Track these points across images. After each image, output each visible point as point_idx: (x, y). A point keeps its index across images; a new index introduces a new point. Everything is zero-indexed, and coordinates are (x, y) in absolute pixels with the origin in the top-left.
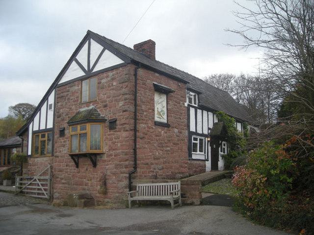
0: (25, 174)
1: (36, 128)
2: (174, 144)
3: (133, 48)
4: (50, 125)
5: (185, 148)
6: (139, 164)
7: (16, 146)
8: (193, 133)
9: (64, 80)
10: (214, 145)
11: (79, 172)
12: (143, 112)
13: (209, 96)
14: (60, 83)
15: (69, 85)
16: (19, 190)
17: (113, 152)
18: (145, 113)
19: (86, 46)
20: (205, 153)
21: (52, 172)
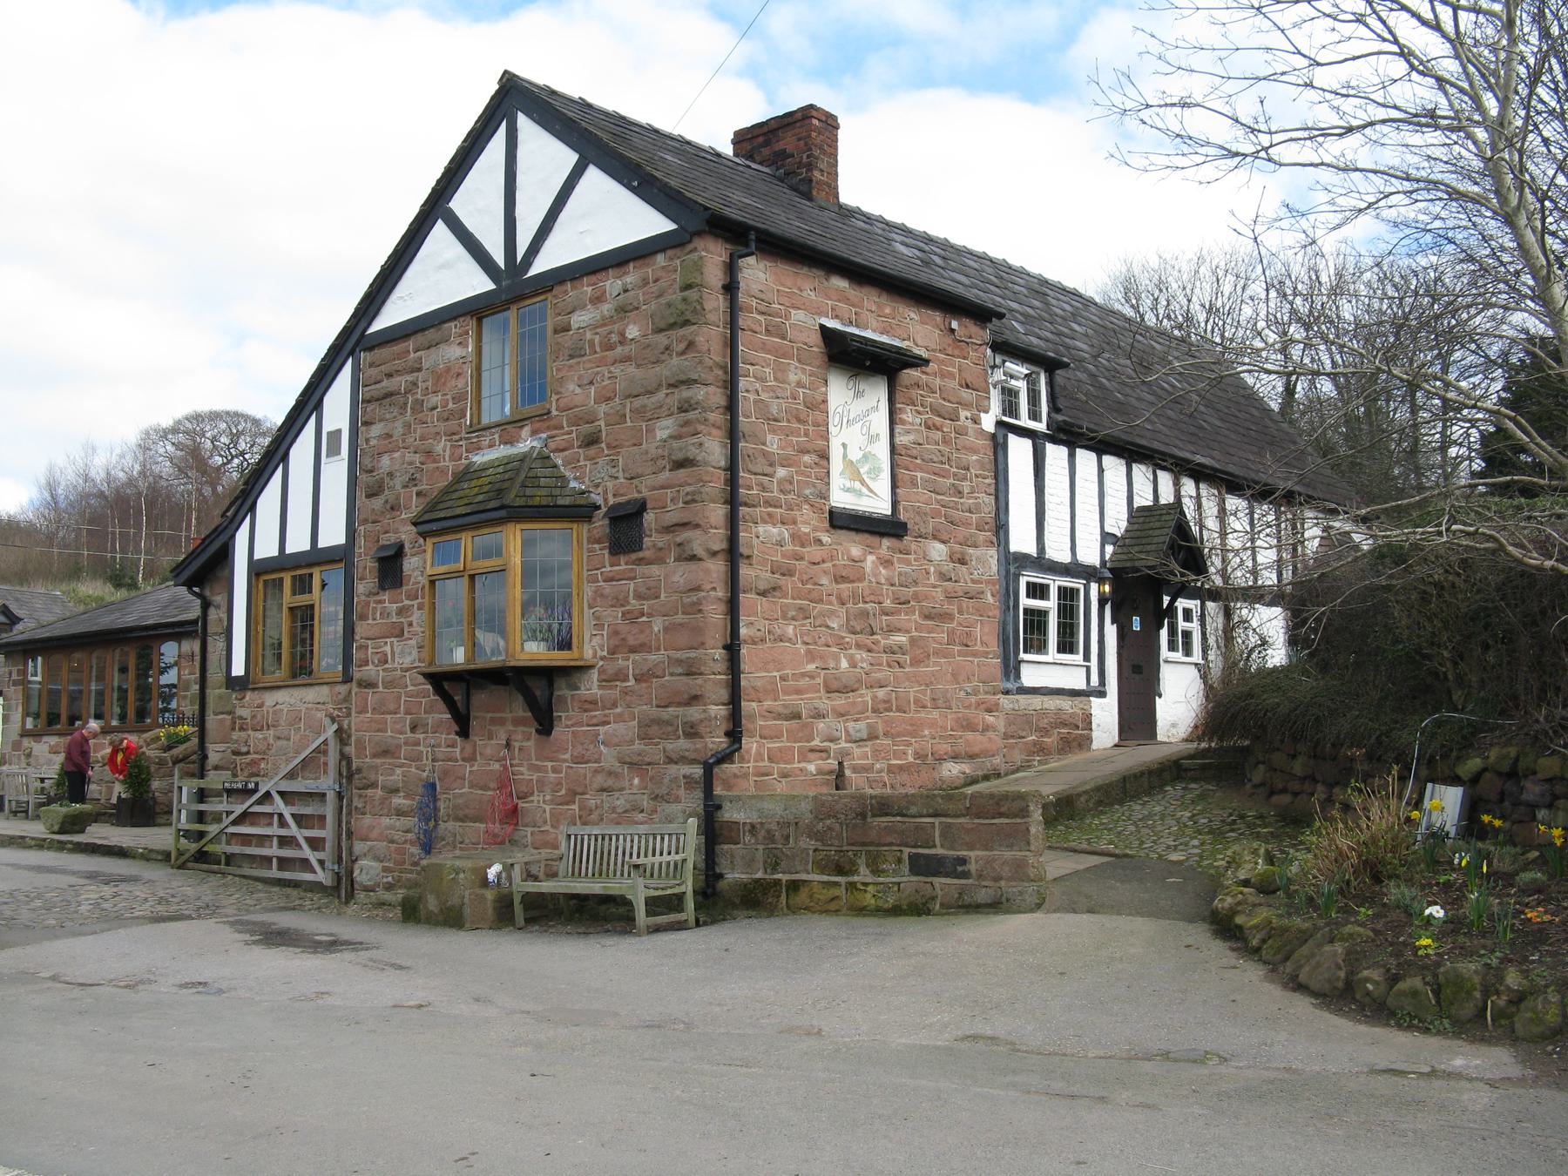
0: (216, 768)
1: (267, 548)
2: (927, 617)
3: (728, 150)
4: (333, 534)
5: (985, 634)
6: (752, 717)
7: (178, 631)
8: (1023, 561)
9: (392, 315)
10: (1136, 620)
11: (471, 759)
13: (1109, 377)
14: (372, 330)
15: (420, 339)
16: (194, 847)
17: (629, 663)
18: (781, 472)
19: (496, 147)
20: (1087, 657)
21: (344, 757)
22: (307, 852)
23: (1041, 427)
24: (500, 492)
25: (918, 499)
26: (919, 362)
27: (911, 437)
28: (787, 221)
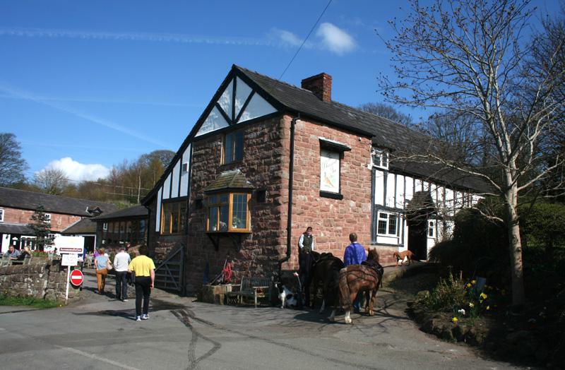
1: (166, 196)
3: (299, 86)
4: (184, 193)
8: (379, 207)
12: (303, 178)
19: (231, 86)
20: (398, 235)
21: (185, 256)
22: (174, 282)
23: (387, 168)
24: (228, 184)
25: (347, 189)
26: (349, 150)
27: (346, 171)
28: (313, 110)
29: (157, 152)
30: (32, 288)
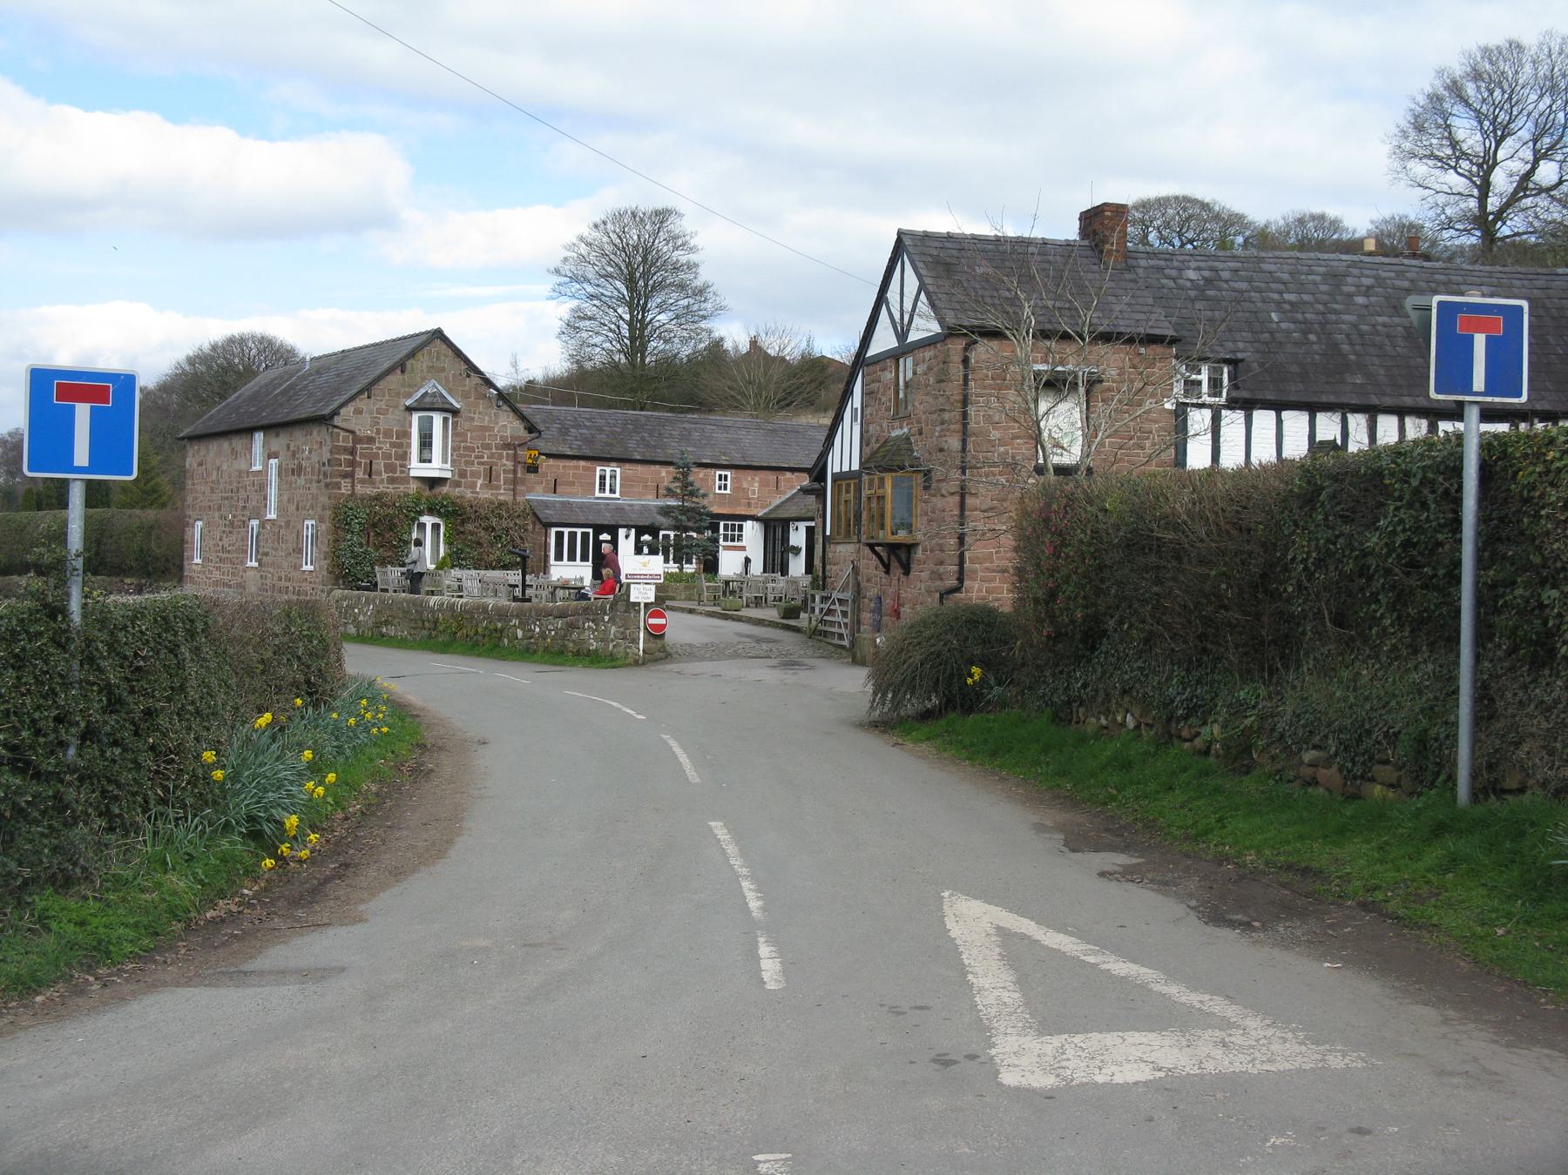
1: (837, 470)
4: (855, 467)
29: (1184, 202)
30: (595, 639)
